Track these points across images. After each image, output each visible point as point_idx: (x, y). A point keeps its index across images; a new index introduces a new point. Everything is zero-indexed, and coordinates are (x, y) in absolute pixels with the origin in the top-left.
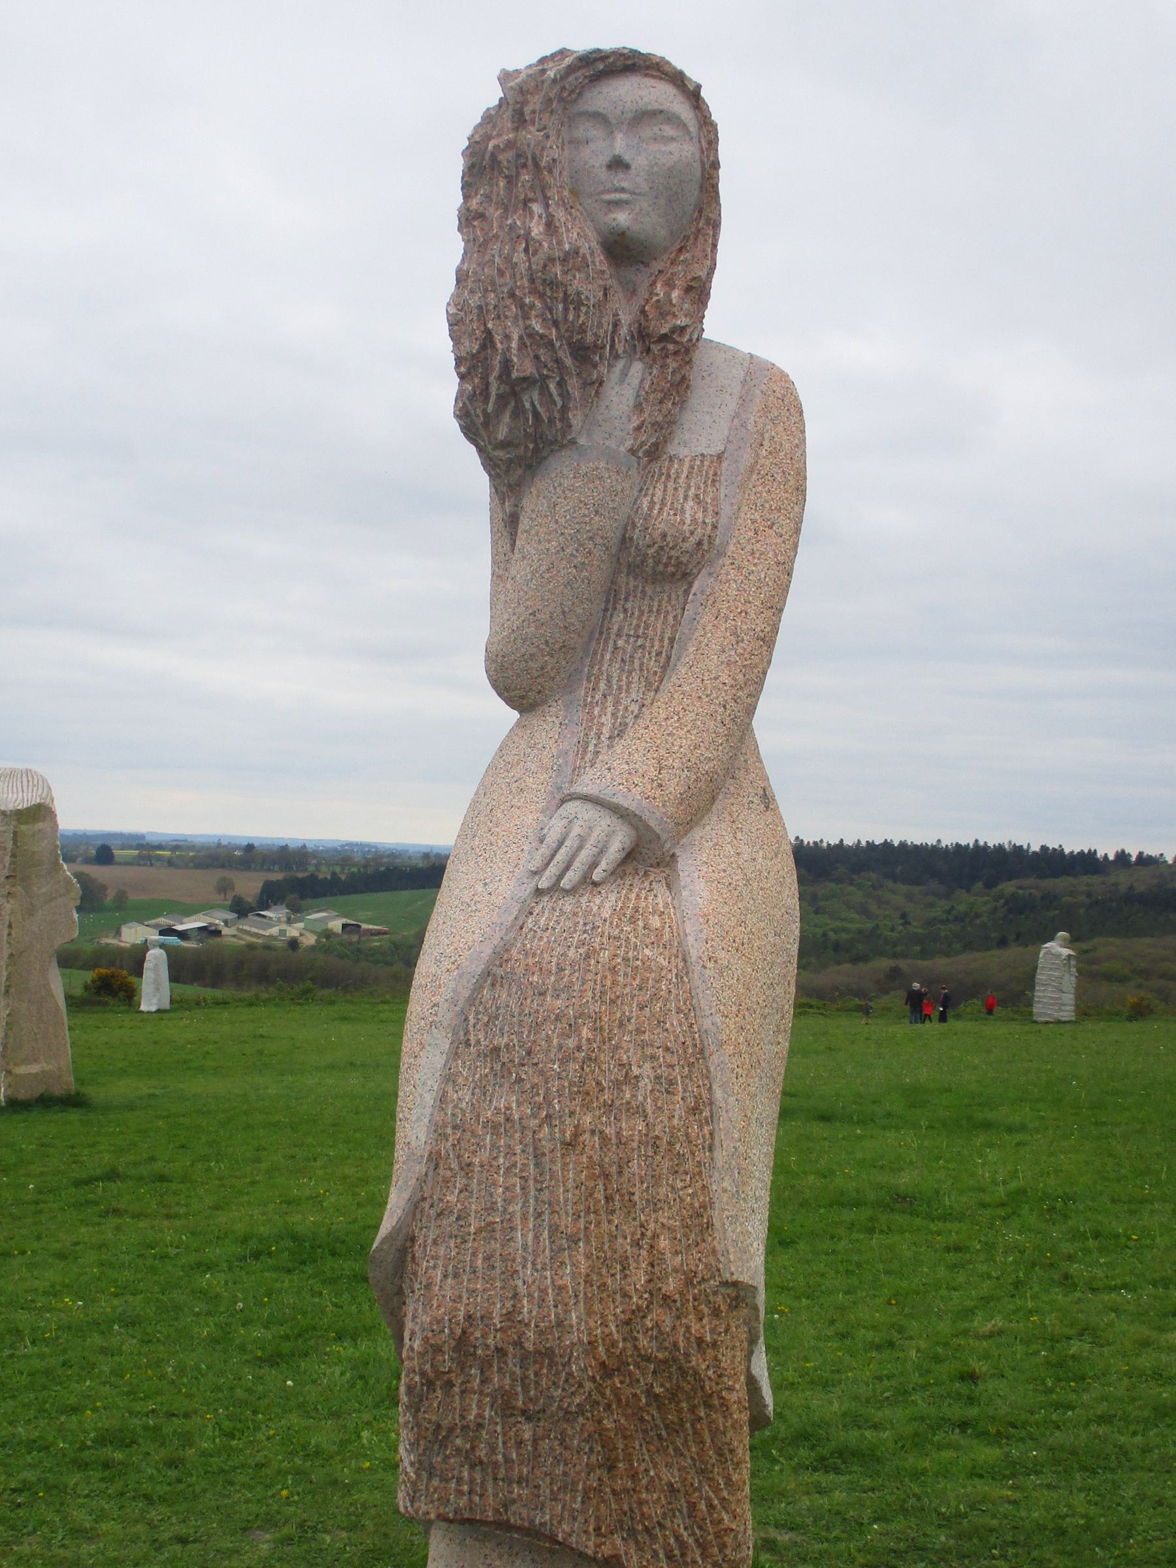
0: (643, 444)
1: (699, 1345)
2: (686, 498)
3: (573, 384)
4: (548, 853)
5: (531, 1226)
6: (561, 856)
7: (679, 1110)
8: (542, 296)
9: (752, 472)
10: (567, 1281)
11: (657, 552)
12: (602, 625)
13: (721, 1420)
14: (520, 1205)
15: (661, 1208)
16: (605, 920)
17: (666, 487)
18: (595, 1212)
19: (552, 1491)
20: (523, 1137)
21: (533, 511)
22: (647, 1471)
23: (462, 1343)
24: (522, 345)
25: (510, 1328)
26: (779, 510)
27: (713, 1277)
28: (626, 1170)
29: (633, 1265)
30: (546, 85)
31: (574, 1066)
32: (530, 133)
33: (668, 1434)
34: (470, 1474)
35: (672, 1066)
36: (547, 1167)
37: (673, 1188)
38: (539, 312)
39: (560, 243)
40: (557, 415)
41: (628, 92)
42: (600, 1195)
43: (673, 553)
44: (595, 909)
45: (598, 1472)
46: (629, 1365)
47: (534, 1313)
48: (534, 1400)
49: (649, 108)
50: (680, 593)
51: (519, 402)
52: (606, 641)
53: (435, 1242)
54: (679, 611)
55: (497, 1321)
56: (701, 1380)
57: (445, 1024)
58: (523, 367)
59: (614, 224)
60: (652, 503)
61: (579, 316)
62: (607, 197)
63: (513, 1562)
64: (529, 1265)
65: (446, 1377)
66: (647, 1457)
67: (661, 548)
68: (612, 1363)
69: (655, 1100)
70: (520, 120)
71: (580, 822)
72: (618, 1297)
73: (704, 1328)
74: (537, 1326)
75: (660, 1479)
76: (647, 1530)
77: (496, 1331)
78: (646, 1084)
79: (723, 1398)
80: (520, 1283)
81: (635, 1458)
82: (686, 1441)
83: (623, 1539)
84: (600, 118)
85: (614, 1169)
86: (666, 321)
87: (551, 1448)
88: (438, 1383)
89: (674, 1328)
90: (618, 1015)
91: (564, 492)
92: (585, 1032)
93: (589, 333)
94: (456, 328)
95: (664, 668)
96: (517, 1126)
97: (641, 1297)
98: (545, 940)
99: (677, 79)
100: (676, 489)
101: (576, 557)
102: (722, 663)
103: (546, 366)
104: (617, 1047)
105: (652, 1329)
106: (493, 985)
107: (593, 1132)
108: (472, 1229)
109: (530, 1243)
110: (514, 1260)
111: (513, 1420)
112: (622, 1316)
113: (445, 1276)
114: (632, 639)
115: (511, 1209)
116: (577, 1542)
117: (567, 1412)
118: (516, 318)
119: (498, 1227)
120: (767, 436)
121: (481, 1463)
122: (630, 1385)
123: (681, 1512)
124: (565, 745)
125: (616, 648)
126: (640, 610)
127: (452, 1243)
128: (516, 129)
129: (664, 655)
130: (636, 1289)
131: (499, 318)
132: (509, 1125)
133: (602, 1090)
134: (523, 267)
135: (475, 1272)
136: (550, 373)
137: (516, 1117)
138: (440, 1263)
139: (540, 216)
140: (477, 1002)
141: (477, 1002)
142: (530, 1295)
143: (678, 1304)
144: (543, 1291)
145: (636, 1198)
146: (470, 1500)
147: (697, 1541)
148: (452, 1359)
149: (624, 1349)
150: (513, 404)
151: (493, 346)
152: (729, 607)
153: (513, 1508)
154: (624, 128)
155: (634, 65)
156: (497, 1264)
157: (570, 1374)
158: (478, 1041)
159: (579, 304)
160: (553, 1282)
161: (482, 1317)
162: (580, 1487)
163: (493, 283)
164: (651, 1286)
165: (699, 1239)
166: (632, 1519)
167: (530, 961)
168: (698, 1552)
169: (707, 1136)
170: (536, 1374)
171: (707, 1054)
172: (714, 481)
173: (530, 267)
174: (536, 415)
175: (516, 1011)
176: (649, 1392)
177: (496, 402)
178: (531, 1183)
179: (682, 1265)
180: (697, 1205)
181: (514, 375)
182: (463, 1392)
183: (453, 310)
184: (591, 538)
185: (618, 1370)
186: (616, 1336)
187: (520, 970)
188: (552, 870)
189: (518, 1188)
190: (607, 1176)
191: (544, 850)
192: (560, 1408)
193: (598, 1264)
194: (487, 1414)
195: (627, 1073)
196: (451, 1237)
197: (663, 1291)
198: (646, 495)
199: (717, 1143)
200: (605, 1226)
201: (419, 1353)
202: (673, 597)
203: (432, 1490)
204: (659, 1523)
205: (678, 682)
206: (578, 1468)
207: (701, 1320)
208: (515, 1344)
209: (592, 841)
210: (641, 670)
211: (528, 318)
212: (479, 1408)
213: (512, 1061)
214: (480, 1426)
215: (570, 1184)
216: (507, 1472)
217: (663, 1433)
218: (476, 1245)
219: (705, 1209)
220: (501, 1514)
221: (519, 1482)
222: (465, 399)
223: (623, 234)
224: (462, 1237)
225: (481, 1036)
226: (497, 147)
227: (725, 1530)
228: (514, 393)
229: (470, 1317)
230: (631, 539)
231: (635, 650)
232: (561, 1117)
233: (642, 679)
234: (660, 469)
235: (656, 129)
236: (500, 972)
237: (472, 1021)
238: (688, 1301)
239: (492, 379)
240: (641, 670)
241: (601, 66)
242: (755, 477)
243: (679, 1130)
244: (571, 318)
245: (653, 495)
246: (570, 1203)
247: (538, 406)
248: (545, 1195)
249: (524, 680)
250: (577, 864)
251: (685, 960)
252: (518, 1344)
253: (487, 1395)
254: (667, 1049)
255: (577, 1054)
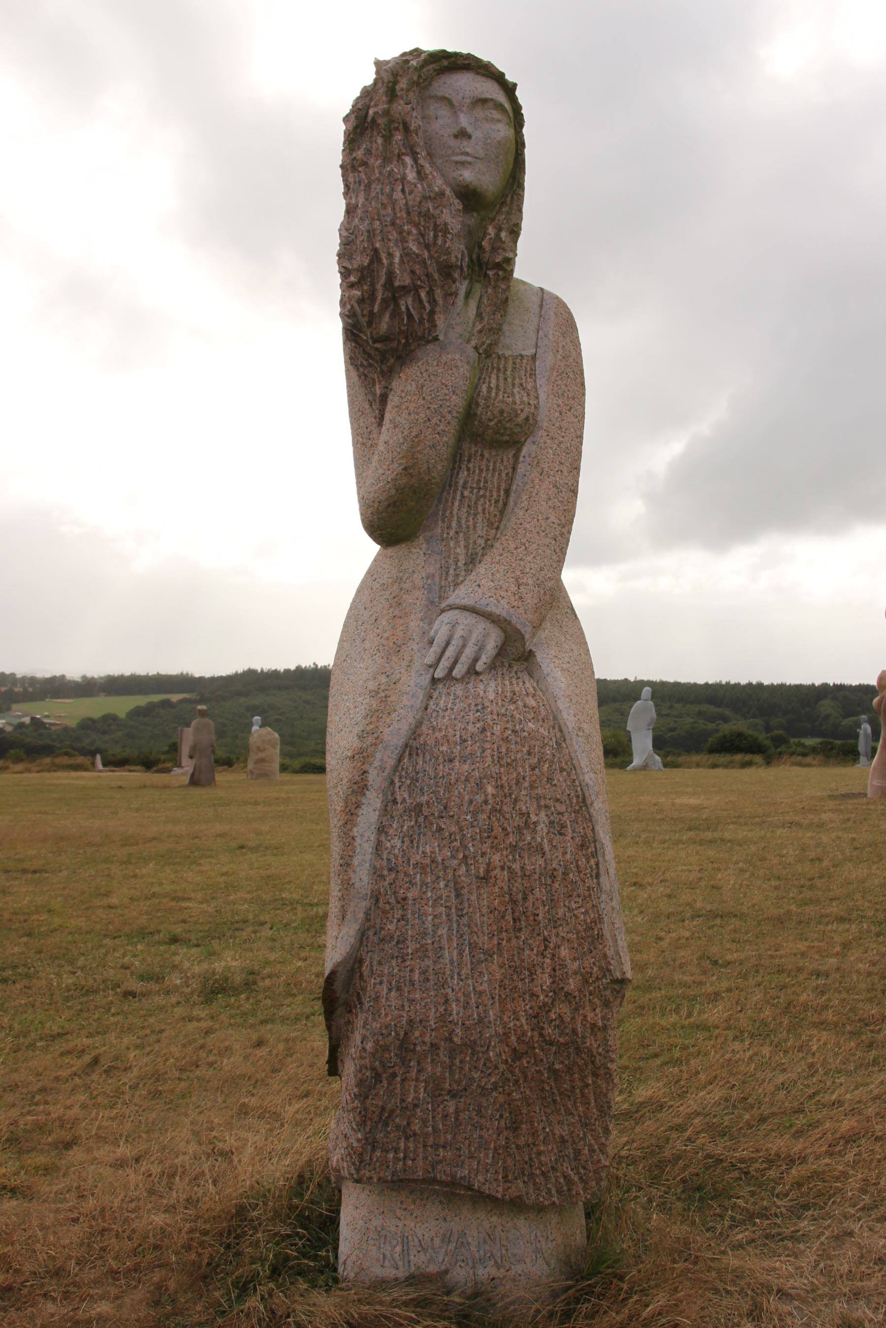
0: (484, 343)
1: (592, 1029)
2: (513, 385)
3: (438, 293)
4: (439, 650)
5: (455, 945)
6: (450, 652)
7: (570, 847)
8: (417, 225)
9: (553, 369)
10: (485, 986)
11: (496, 424)
12: (451, 481)
13: (604, 1086)
14: (446, 929)
15: (561, 925)
16: (492, 701)
18: (506, 931)
19: (470, 1151)
20: (446, 874)
21: (402, 391)
22: (544, 1128)
23: (405, 1046)
24: (402, 261)
25: (442, 1027)
26: (574, 398)
27: (604, 976)
28: (530, 897)
29: (539, 971)
30: (410, 71)
31: (483, 816)
32: (400, 105)
33: (561, 1099)
34: (405, 1144)
35: (561, 813)
36: (466, 897)
37: (569, 909)
38: (415, 238)
39: (429, 186)
40: (425, 316)
41: (465, 84)
42: (509, 917)
44: (482, 693)
45: (506, 1133)
46: (534, 1048)
47: (461, 1014)
48: (459, 1082)
50: (510, 456)
51: (397, 305)
52: (455, 491)
53: (380, 963)
54: (510, 470)
55: (432, 1023)
56: (592, 1056)
57: (376, 787)
59: (461, 178)
60: (490, 388)
61: (445, 242)
63: (425, 1205)
64: (456, 977)
65: (391, 1071)
66: (544, 1118)
67: (500, 421)
68: (522, 1048)
69: (550, 841)
70: (392, 94)
71: (461, 627)
72: (527, 996)
73: (595, 1016)
74: (463, 1024)
75: (554, 1134)
76: (543, 1173)
77: (432, 1030)
78: (542, 828)
79: (608, 1068)
80: (449, 991)
81: (536, 1120)
82: (575, 1103)
83: (524, 1182)
84: (447, 101)
85: (520, 896)
86: (499, 254)
87: (470, 1118)
88: (384, 1075)
89: (573, 1018)
90: (515, 775)
91: (429, 376)
92: (490, 789)
93: (453, 255)
94: (348, 247)
95: (502, 512)
96: (440, 867)
97: (547, 996)
98: (447, 718)
99: (498, 78)
100: (505, 379)
102: (550, 507)
103: (419, 279)
104: (516, 801)
105: (555, 1020)
106: (410, 754)
107: (502, 868)
108: (410, 951)
109: (455, 959)
110: (444, 973)
111: (440, 1099)
112: (531, 1011)
113: (390, 990)
114: (475, 491)
115: (439, 933)
116: (489, 1189)
117: (483, 1088)
118: (397, 240)
119: (430, 947)
120: (560, 345)
121: (415, 1134)
122: (535, 1064)
123: (568, 1157)
124: (431, 570)
126: (480, 469)
127: (394, 963)
128: (390, 102)
130: (542, 989)
132: (434, 865)
133: (507, 834)
135: (413, 985)
136: (422, 284)
137: (440, 859)
138: (385, 979)
140: (400, 769)
141: (400, 769)
142: (458, 1000)
143: (577, 999)
144: (467, 995)
145: (540, 917)
146: (405, 1164)
147: (581, 1178)
148: (396, 1055)
149: (532, 1037)
150: (392, 307)
151: (379, 260)
152: (549, 467)
153: (439, 1167)
156: (431, 978)
157: (488, 1059)
158: (404, 799)
159: (446, 231)
160: (474, 989)
161: (421, 1021)
162: (492, 1146)
163: (379, 214)
164: (555, 986)
165: (592, 948)
166: (531, 1166)
167: (438, 735)
168: (581, 1186)
169: (594, 867)
170: (461, 1062)
171: (589, 802)
172: (531, 374)
173: (407, 204)
174: (410, 316)
175: (432, 774)
176: (551, 1069)
177: (381, 305)
178: (453, 910)
179: (580, 968)
180: (589, 921)
181: (397, 284)
182: (403, 1080)
183: (345, 234)
184: (450, 412)
185: (526, 1053)
186: (526, 1027)
187: (431, 742)
188: (445, 664)
189: (444, 915)
190: (514, 902)
191: (435, 649)
192: (479, 1086)
193: (511, 971)
194: (421, 1096)
195: (526, 821)
196: (392, 958)
197: (566, 990)
198: (484, 383)
199: (602, 871)
200: (514, 942)
201: (372, 1053)
202: (505, 459)
203: (375, 1159)
204: (553, 1168)
205: (519, 522)
206: (490, 1132)
207: (594, 1010)
208: (446, 1039)
209: (473, 640)
210: (484, 513)
211: (407, 242)
212: (415, 1092)
213: (433, 814)
214: (416, 1106)
215: (485, 910)
216: (435, 1139)
217: (558, 1098)
218: (413, 963)
219: (596, 924)
220: (429, 1172)
221: (444, 1147)
222: (353, 302)
223: (467, 186)
224: (402, 958)
225: (406, 795)
226: (376, 113)
227: (602, 1167)
229: (411, 1021)
230: (476, 414)
231: (478, 499)
232: (475, 857)
234: (492, 364)
236: (415, 744)
237: (398, 785)
238: (585, 995)
239: (379, 286)
240: (484, 513)
241: (445, 63)
242: (555, 374)
243: (572, 863)
244: (440, 242)
245: (490, 383)
246: (485, 925)
247: (412, 310)
248: (465, 920)
249: (394, 518)
250: (463, 659)
251: (561, 730)
252: (449, 1039)
253: (422, 1082)
254: (557, 800)
255: (484, 807)
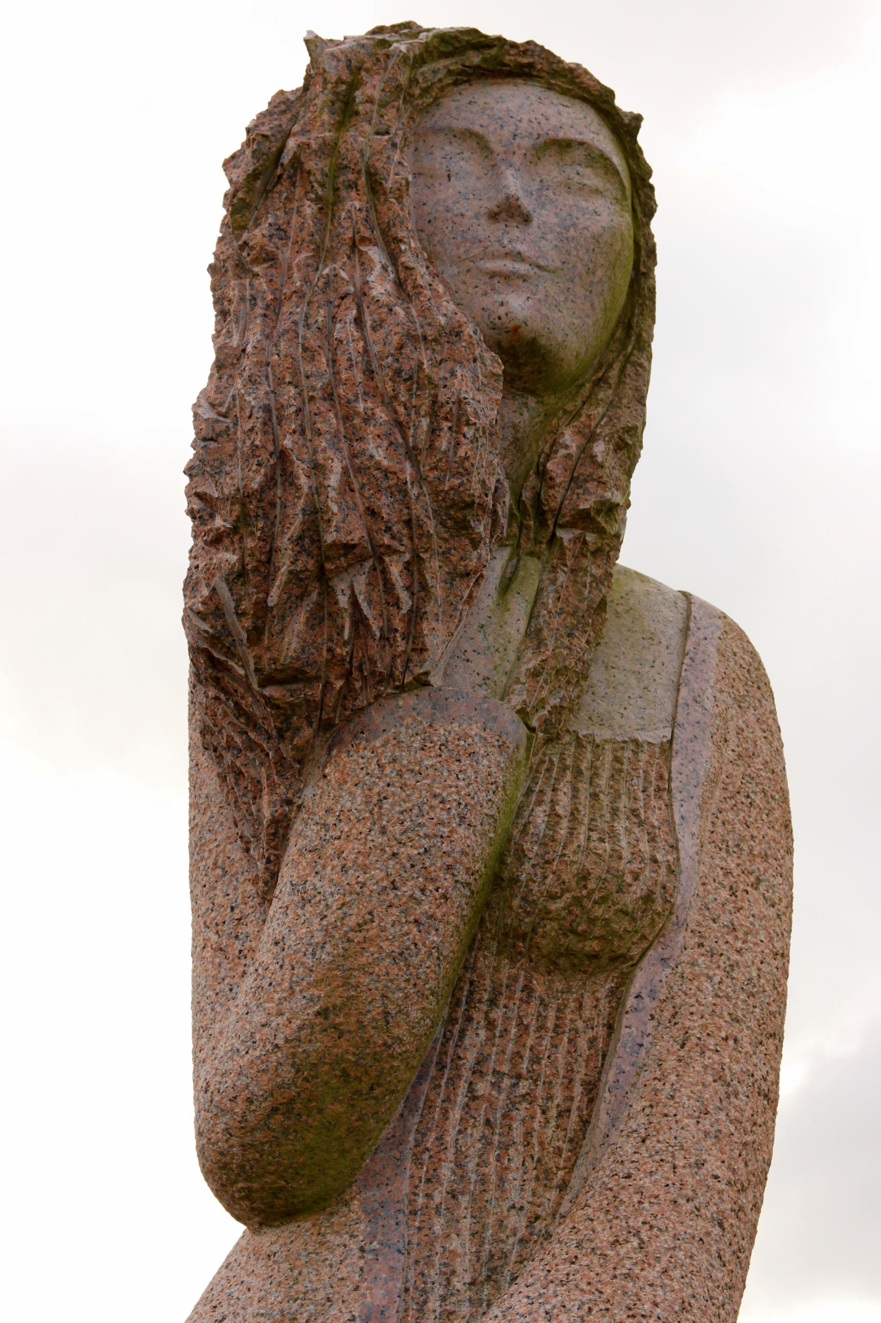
0: (542, 702)
2: (615, 812)
3: (435, 570)
8: (389, 402)
11: (568, 908)
17: (575, 790)
24: (347, 486)
26: (765, 857)
32: (362, 133)
38: (384, 429)
40: (398, 624)
43: (599, 911)
49: (561, 135)
50: (602, 993)
51: (328, 592)
52: (453, 1081)
54: (601, 1032)
58: (345, 526)
59: (502, 311)
60: (553, 815)
62: (490, 265)
70: (345, 108)
84: (478, 141)
91: (400, 774)
94: (213, 445)
95: (576, 1143)
99: (599, 100)
100: (595, 796)
101: (419, 902)
114: (507, 1082)
120: (731, 725)
125: (474, 1098)
126: (520, 1024)
129: (574, 1116)
131: (303, 432)
134: (354, 348)
139: (384, 268)
152: (704, 1027)
154: (517, 160)
155: (531, 65)
172: (659, 789)
173: (366, 351)
174: (359, 621)
183: (208, 414)
198: (539, 803)
202: (588, 1001)
205: (622, 1170)
211: (361, 439)
228: (322, 576)
230: (515, 880)
231: (513, 1105)
233: (530, 1164)
234: (562, 759)
235: (570, 171)
239: (284, 542)
241: (475, 58)
247: (364, 606)
